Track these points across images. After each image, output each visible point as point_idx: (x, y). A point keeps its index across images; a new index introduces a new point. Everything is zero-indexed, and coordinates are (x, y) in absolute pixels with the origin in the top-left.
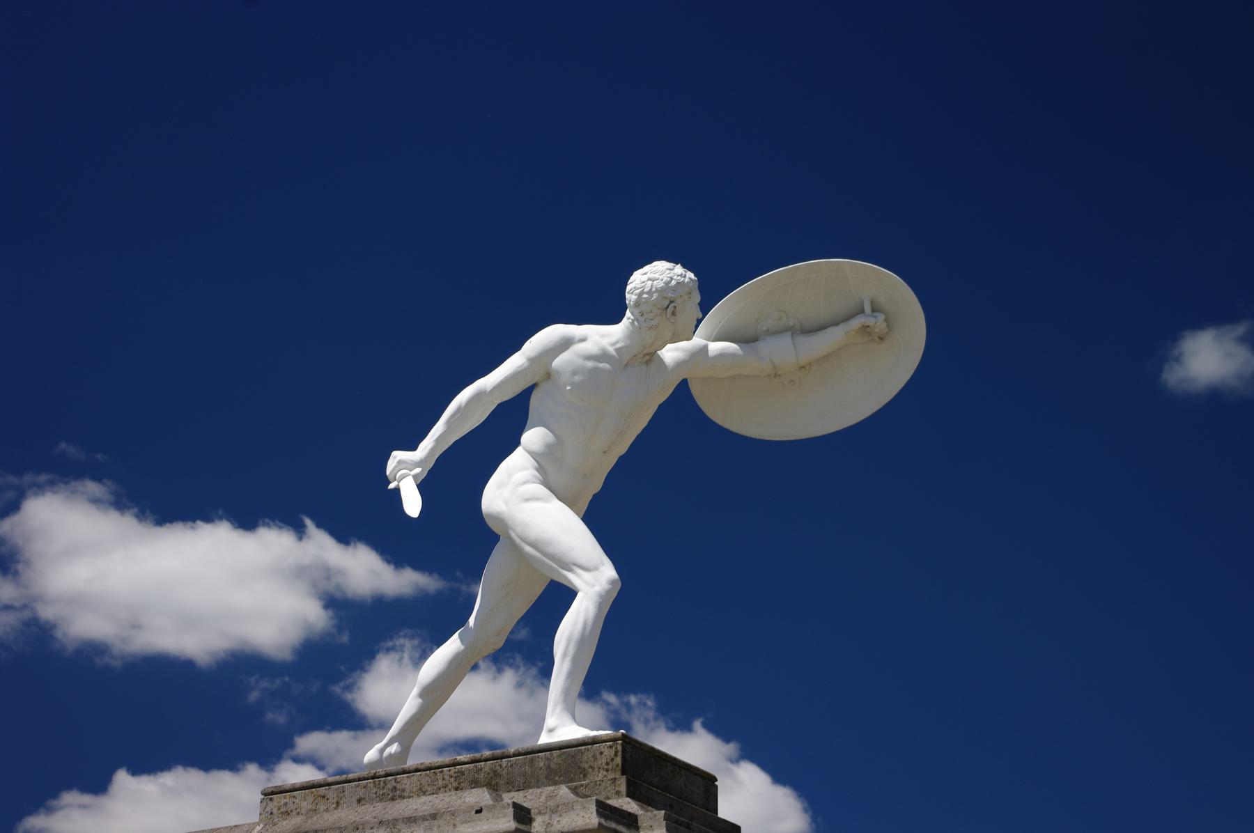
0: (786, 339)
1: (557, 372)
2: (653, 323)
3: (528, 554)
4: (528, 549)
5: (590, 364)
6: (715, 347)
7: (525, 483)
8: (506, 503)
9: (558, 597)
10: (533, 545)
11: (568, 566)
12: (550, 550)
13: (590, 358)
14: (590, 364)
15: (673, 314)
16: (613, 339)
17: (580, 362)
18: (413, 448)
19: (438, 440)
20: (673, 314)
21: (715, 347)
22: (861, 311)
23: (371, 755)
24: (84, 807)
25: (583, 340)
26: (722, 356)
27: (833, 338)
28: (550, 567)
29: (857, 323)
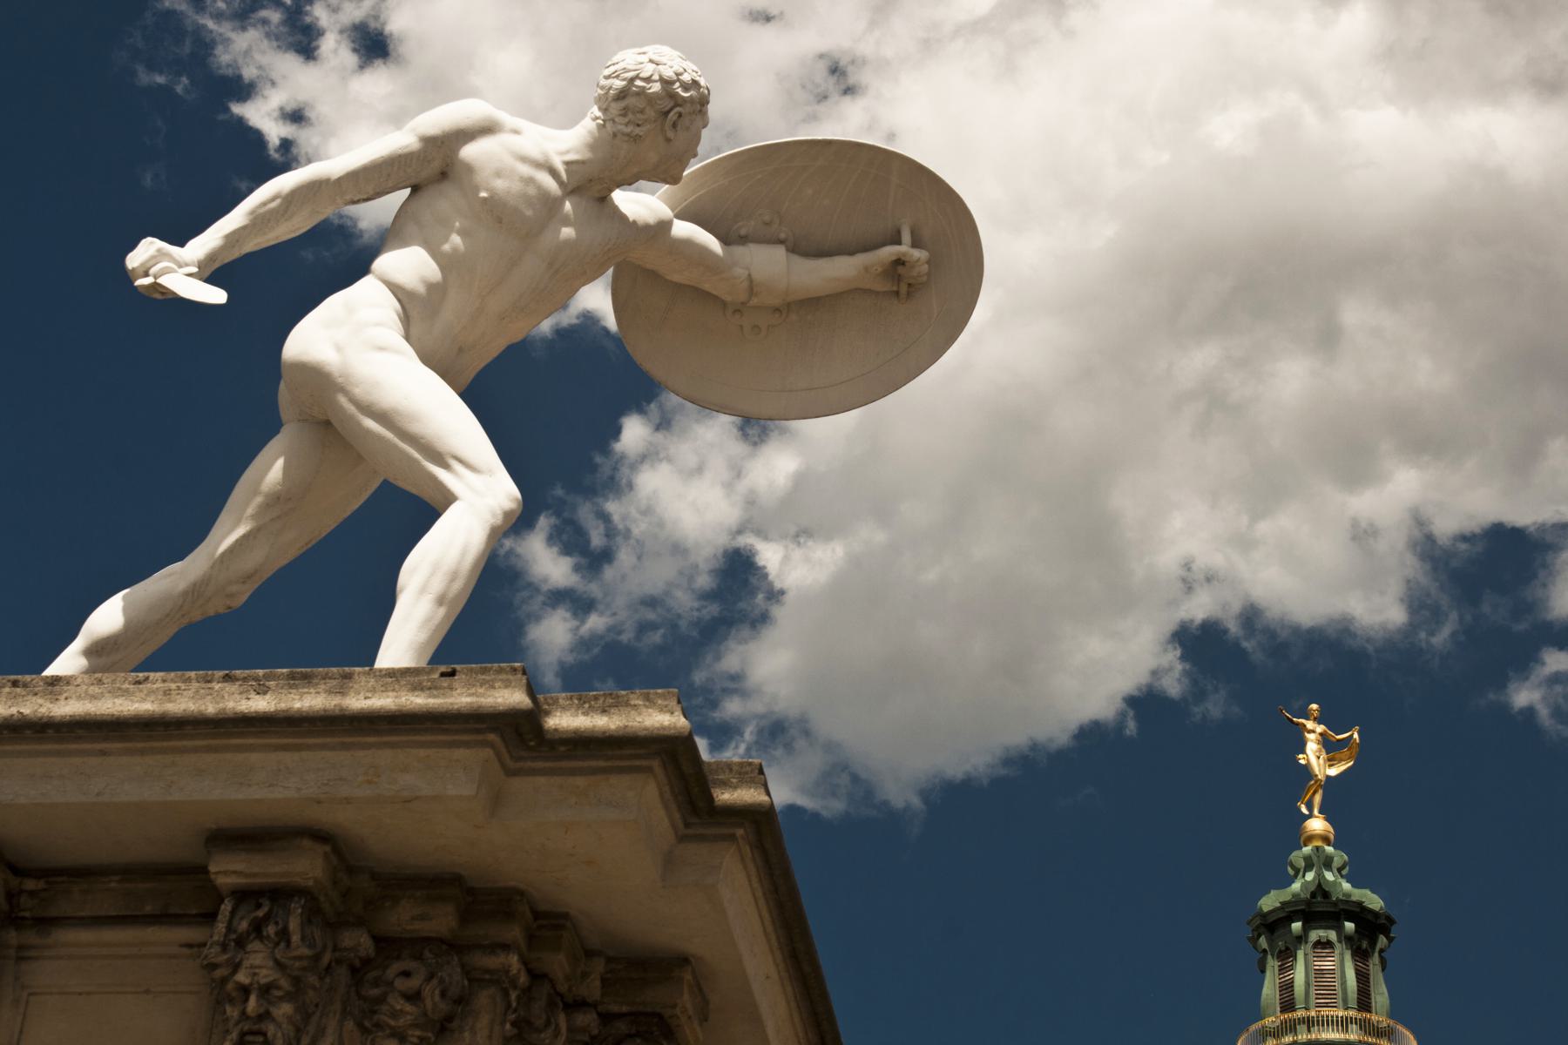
0: (779, 252)
1: (469, 169)
2: (637, 131)
3: (368, 432)
4: (370, 424)
5: (526, 170)
6: (684, 229)
7: (377, 325)
8: (339, 349)
9: (416, 511)
10: (384, 417)
11: (440, 459)
12: (415, 428)
13: (524, 159)
14: (526, 170)
15: (674, 125)
16: (564, 147)
17: (510, 161)
18: (182, 244)
19: (233, 238)
20: (674, 125)
21: (684, 229)
22: (897, 241)
23: (931, 576)
24: (743, 860)
25: (516, 132)
26: (688, 244)
27: (842, 269)
28: (402, 452)
29: (889, 252)
